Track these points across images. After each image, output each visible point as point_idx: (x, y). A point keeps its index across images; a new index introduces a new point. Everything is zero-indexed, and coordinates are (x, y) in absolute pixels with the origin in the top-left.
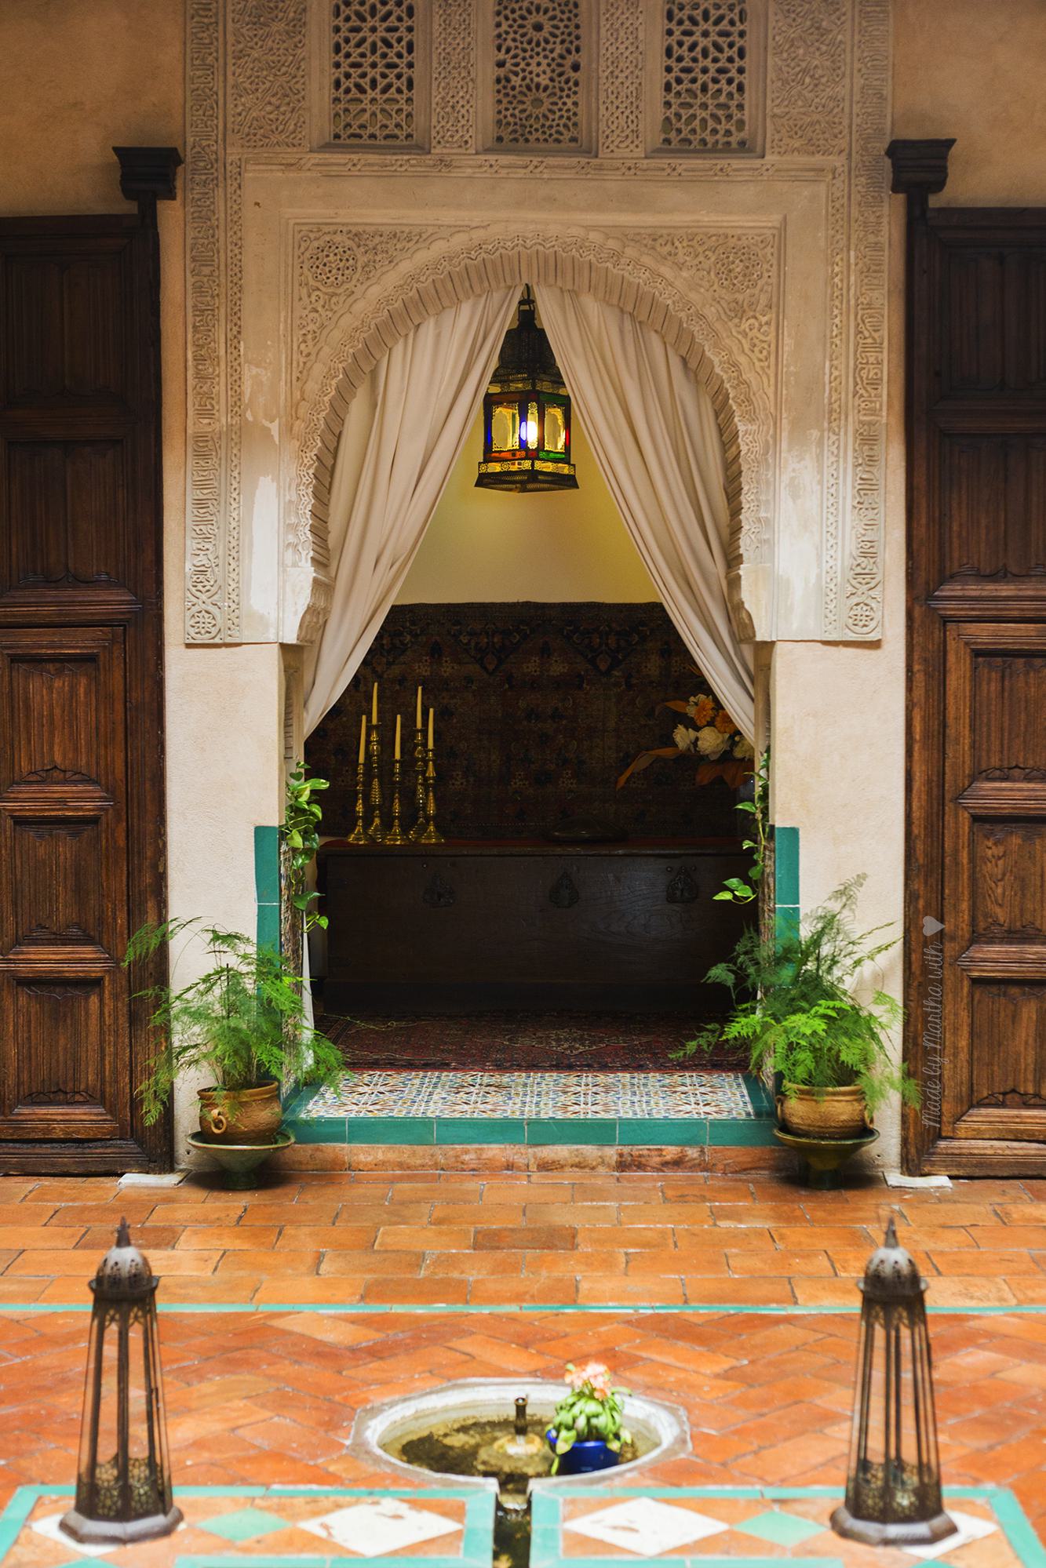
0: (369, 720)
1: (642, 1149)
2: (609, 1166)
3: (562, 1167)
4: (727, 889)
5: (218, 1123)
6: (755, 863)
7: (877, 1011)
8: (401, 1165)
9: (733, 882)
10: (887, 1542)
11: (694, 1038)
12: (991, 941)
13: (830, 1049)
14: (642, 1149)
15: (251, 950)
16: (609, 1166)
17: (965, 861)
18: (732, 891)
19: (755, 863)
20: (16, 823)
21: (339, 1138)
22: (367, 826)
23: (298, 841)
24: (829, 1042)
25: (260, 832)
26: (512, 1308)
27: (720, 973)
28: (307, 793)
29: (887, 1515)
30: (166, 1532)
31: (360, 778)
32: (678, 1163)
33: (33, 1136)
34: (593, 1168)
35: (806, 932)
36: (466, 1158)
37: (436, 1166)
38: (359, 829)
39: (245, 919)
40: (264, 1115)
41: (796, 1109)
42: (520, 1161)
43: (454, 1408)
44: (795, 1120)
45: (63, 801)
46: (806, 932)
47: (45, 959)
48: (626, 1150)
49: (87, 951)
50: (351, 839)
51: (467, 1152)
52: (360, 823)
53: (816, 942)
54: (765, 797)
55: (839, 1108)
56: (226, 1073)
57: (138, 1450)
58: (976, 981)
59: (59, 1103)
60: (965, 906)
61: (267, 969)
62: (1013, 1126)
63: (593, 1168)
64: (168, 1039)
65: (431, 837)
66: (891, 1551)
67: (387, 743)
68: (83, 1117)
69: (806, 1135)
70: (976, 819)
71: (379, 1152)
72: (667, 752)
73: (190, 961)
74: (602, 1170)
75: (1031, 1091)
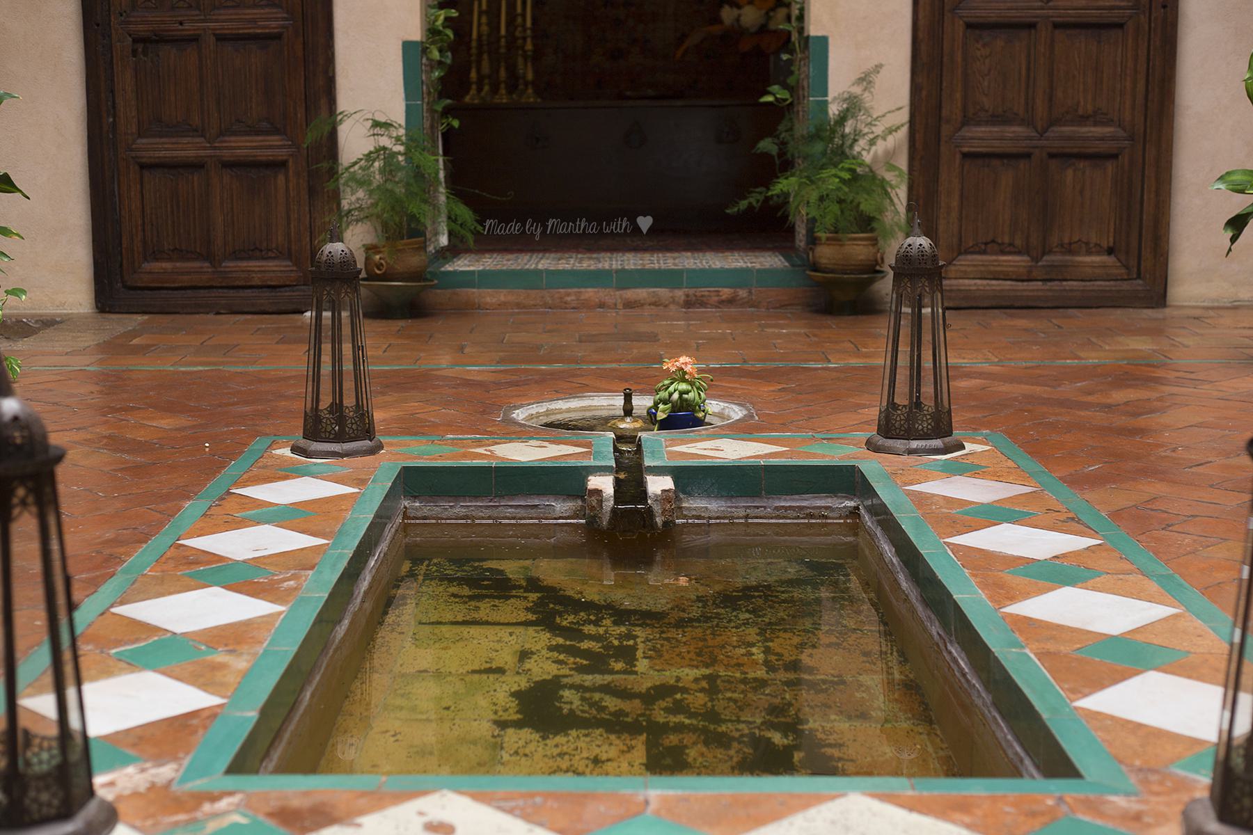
0: (480, 5)
1: (704, 291)
2: (678, 304)
3: (642, 305)
4: (769, 93)
5: (379, 266)
6: (792, 73)
7: (889, 176)
8: (518, 305)
9: (775, 88)
10: (911, 452)
11: (745, 198)
12: (978, 124)
13: (852, 202)
14: (704, 291)
15: (402, 132)
16: (678, 304)
17: (959, 60)
18: (774, 95)
19: (792, 73)
20: (218, 40)
21: (471, 284)
22: (480, 90)
23: (436, 55)
24: (851, 197)
25: (407, 46)
26: (614, 365)
27: (767, 145)
28: (442, 18)
29: (909, 435)
30: (373, 451)
31: (474, 51)
32: (731, 301)
33: (238, 283)
34: (666, 306)
35: (834, 110)
36: (569, 299)
37: (545, 305)
38: (473, 91)
39: (395, 109)
40: (415, 261)
41: (825, 254)
42: (610, 301)
43: (575, 410)
44: (824, 261)
45: (254, 21)
46: (834, 110)
47: (243, 146)
48: (691, 291)
49: (275, 140)
50: (467, 99)
51: (569, 295)
52: (474, 87)
53: (842, 119)
54: (801, 18)
55: (858, 250)
56: (385, 226)
57: (349, 401)
58: (966, 156)
59: (257, 259)
60: (958, 95)
61: (412, 142)
62: (992, 268)
63: (666, 306)
64: (339, 204)
65: (530, 97)
66: (913, 458)
67: (495, 27)
68: (275, 268)
69: (832, 271)
70: (969, 26)
71: (502, 296)
72: (716, 29)
73: (354, 142)
74: (672, 307)
75: (1007, 240)
